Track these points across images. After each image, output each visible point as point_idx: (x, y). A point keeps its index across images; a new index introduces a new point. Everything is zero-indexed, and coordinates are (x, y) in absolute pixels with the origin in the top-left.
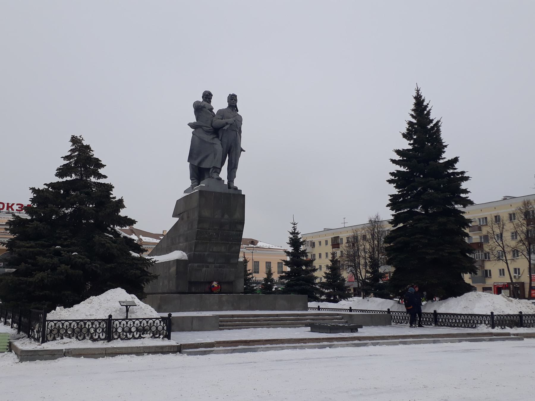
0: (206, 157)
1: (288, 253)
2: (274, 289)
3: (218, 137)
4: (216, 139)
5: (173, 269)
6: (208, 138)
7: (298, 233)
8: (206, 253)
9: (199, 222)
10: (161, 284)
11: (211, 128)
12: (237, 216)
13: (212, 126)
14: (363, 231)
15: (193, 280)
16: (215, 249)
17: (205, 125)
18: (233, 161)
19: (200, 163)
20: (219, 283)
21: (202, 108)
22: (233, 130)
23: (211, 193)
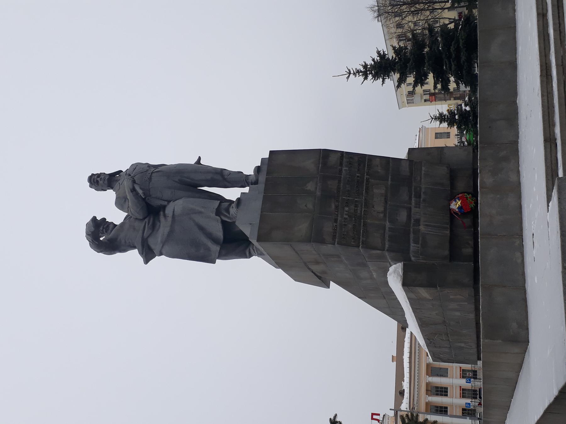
0: (202, 229)
1: (401, 81)
2: (468, 108)
3: (164, 208)
4: (167, 212)
5: (423, 293)
6: (164, 226)
7: (365, 66)
8: (388, 224)
9: (322, 241)
10: (458, 314)
11: (147, 220)
12: (310, 164)
13: (144, 218)
14: (392, 26)
15: (447, 252)
17: (141, 232)
18: (209, 177)
19: (215, 241)
20: (453, 198)
21: (103, 237)
22: (150, 179)
23: (263, 218)
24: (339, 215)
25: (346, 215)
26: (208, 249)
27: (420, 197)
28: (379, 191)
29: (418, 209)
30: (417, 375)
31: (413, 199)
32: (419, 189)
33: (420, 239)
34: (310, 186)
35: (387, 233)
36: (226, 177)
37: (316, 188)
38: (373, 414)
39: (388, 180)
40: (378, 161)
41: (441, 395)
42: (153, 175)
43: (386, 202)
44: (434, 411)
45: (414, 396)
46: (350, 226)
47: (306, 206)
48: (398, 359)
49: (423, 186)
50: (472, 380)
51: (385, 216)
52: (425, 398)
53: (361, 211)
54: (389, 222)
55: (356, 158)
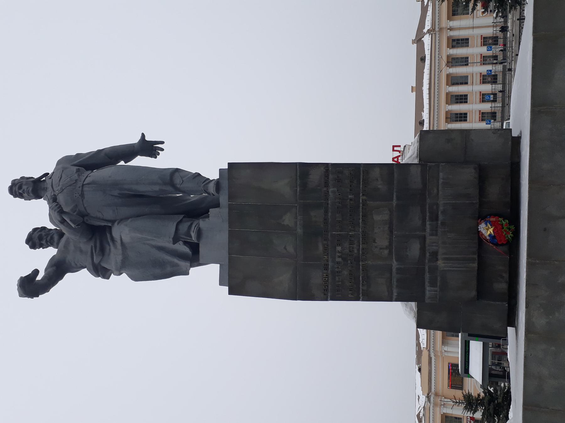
15: (474, 293)
16: (382, 241)
22: (82, 195)
24: (330, 260)
25: (339, 257)
26: (177, 265)
27: (437, 219)
28: (380, 217)
29: (434, 237)
30: (436, 105)
31: (428, 223)
32: (435, 207)
33: (439, 279)
34: (288, 220)
35: (395, 276)
36: (178, 186)
37: (296, 223)
38: (394, 147)
39: (392, 200)
40: (377, 172)
41: (461, 102)
42: (85, 189)
43: (391, 232)
44: (454, 119)
45: (434, 106)
46: (345, 273)
47: (285, 248)
48: (418, 89)
49: (441, 202)
50: (493, 47)
51: (390, 253)
52: (445, 108)
53: (358, 250)
54: (397, 261)
55: (346, 172)
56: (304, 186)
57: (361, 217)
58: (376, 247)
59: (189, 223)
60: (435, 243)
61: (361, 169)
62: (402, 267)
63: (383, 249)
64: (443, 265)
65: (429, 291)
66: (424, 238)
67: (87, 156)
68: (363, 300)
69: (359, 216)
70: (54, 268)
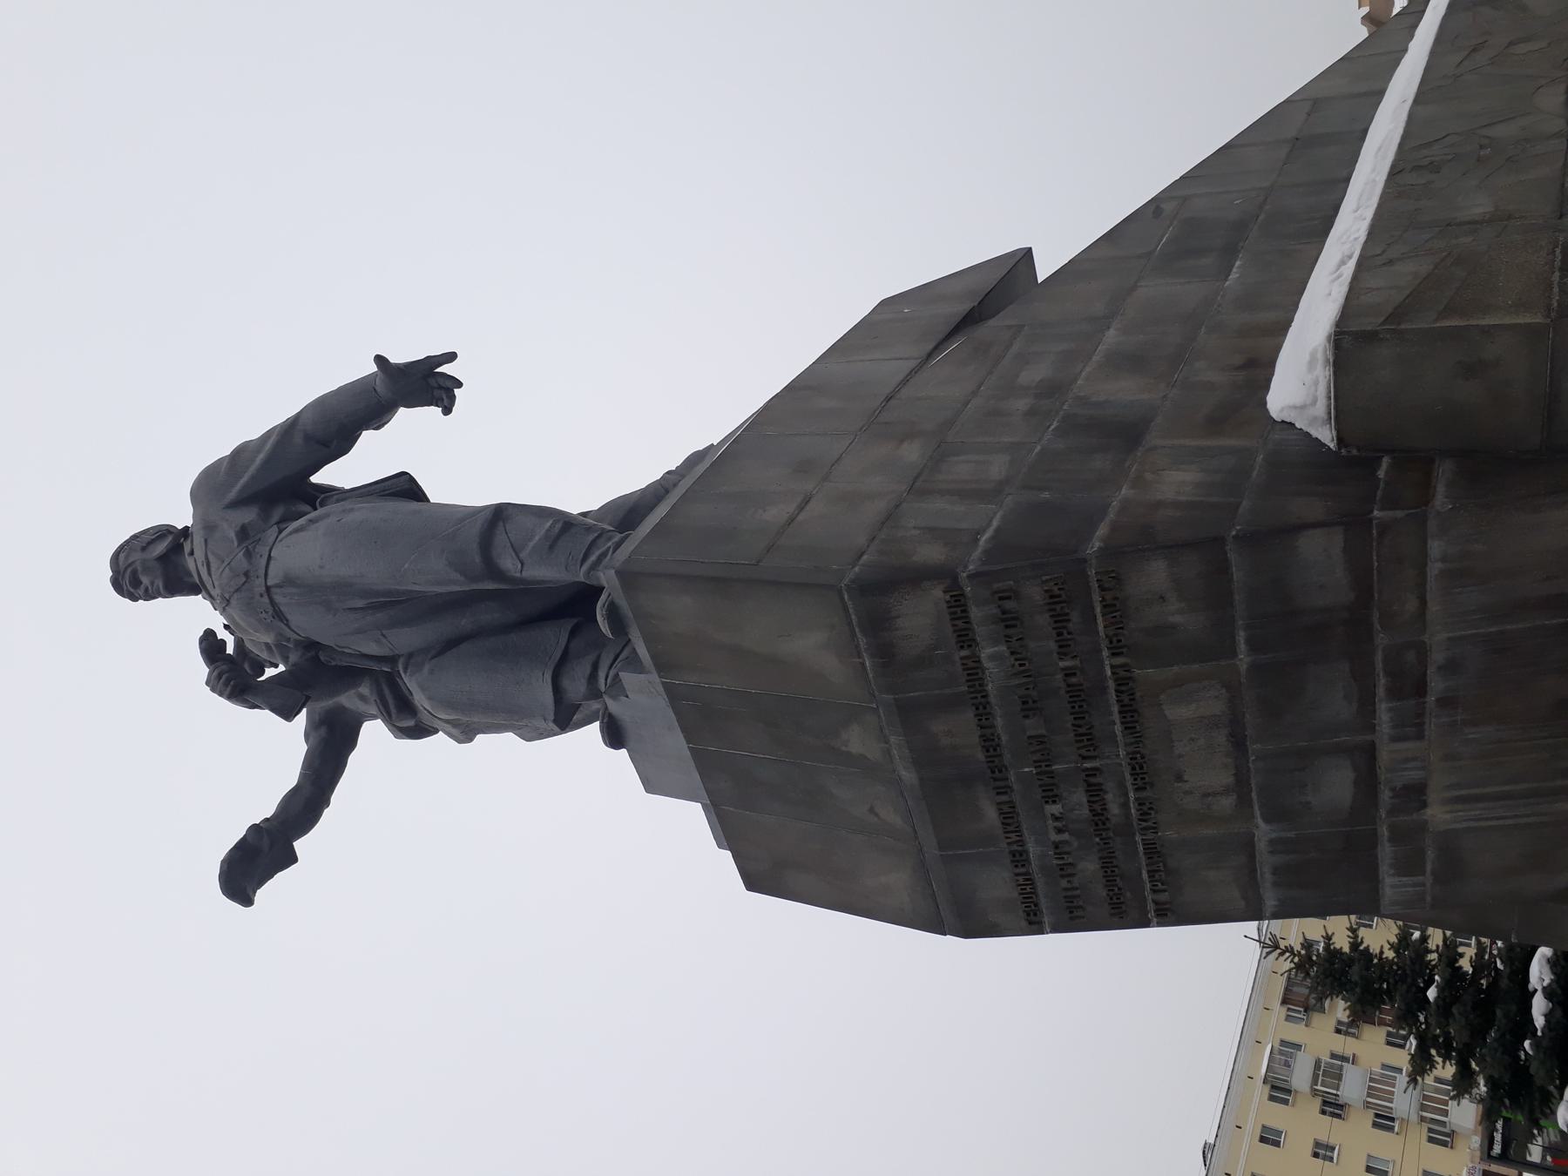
27: (1421, 689)
29: (1410, 746)
32: (1411, 656)
33: (1430, 854)
35: (1266, 861)
37: (888, 752)
39: (1234, 654)
47: (872, 810)
49: (1438, 638)
51: (1244, 801)
53: (1125, 805)
54: (1267, 820)
56: (886, 654)
57: (1116, 717)
58: (1186, 793)
59: (591, 658)
60: (1414, 759)
61: (1092, 572)
62: (1292, 834)
63: (1215, 794)
64: (1448, 816)
65: (1392, 887)
66: (1371, 751)
67: (268, 446)
68: (1160, 924)
69: (1111, 714)
70: (323, 731)
